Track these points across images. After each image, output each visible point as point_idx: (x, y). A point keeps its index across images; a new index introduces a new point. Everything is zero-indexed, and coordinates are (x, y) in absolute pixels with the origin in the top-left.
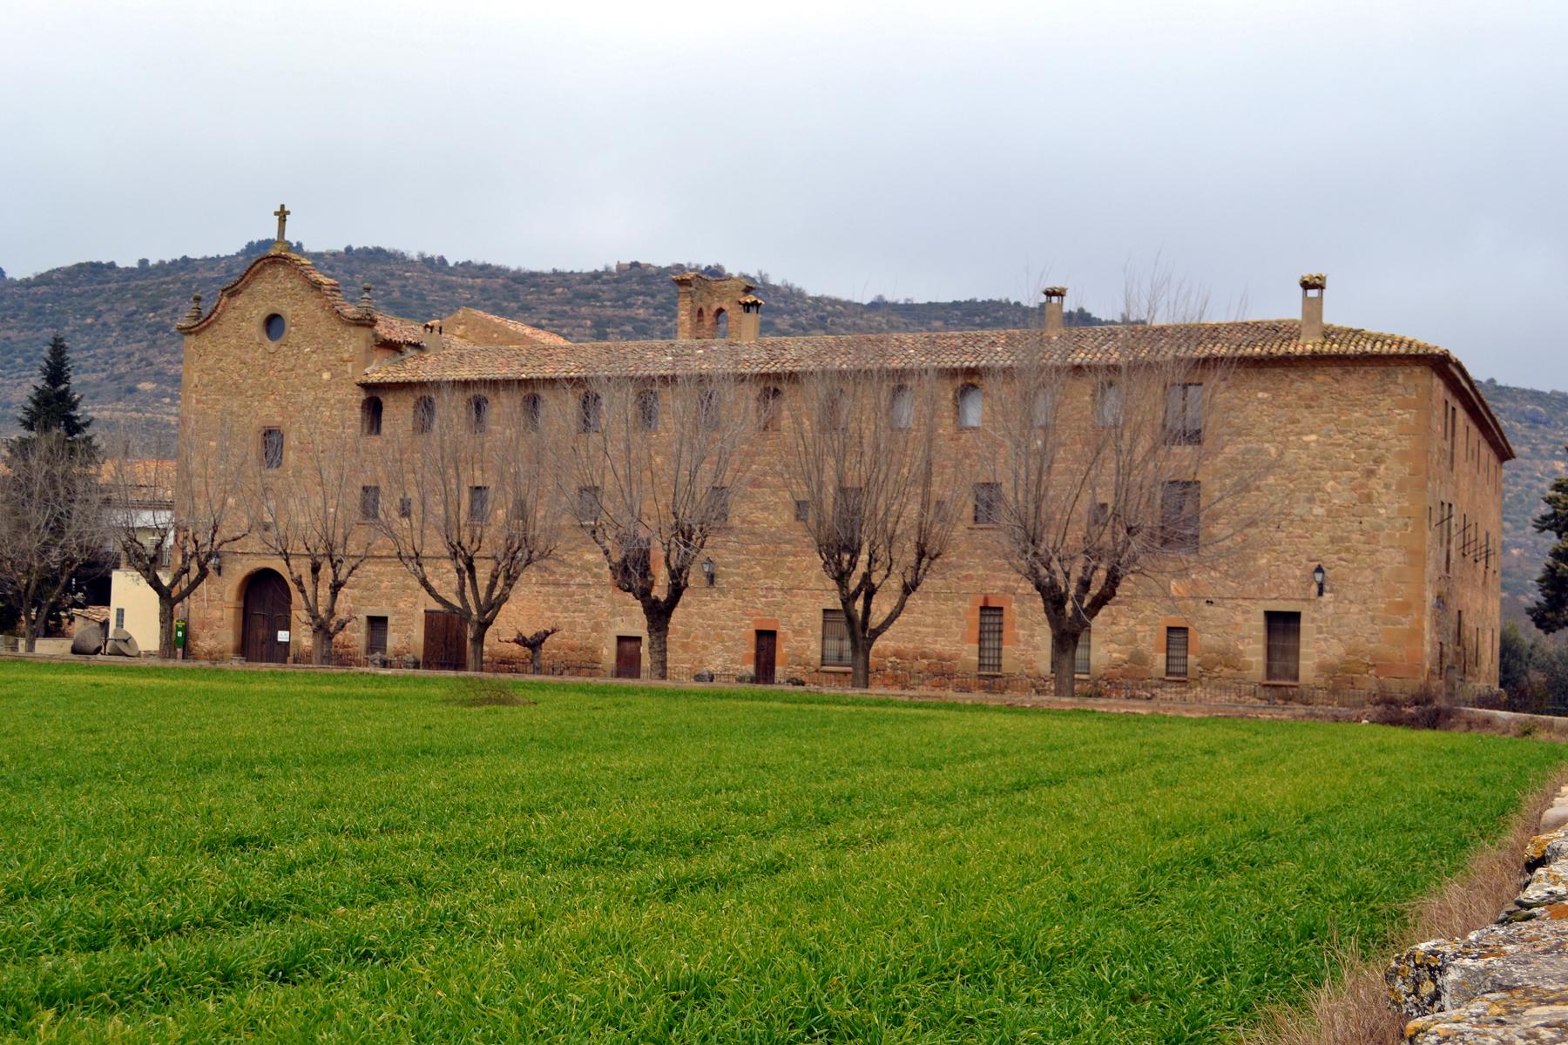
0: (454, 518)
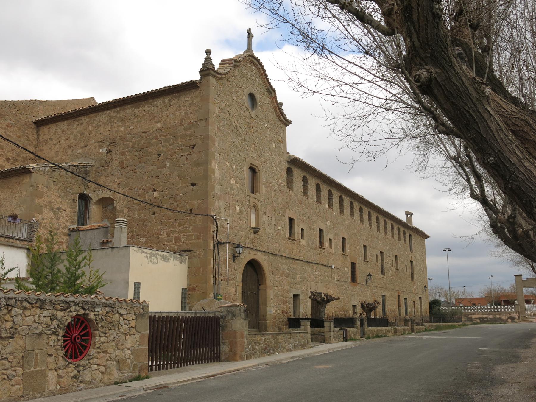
0: (216, 247)
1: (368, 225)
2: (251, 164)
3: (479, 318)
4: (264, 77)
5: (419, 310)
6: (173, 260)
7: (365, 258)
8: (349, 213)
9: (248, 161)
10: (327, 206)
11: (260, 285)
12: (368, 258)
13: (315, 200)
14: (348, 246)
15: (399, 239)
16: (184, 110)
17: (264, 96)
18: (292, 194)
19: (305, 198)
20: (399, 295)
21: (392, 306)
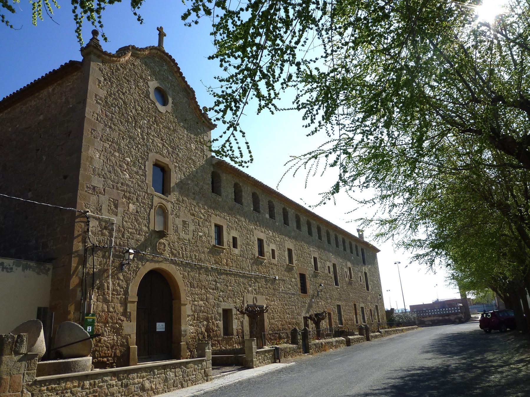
1: (317, 238)
2: (156, 160)
3: (431, 321)
4: (179, 75)
5: (377, 317)
6: (23, 270)
7: (315, 270)
8: (295, 225)
9: (153, 156)
10: (267, 216)
11: (173, 300)
12: (319, 269)
13: (252, 209)
14: (294, 257)
15: (352, 252)
16: (65, 96)
17: (180, 95)
18: (220, 200)
19: (238, 205)
20: (355, 305)
21: (348, 315)
